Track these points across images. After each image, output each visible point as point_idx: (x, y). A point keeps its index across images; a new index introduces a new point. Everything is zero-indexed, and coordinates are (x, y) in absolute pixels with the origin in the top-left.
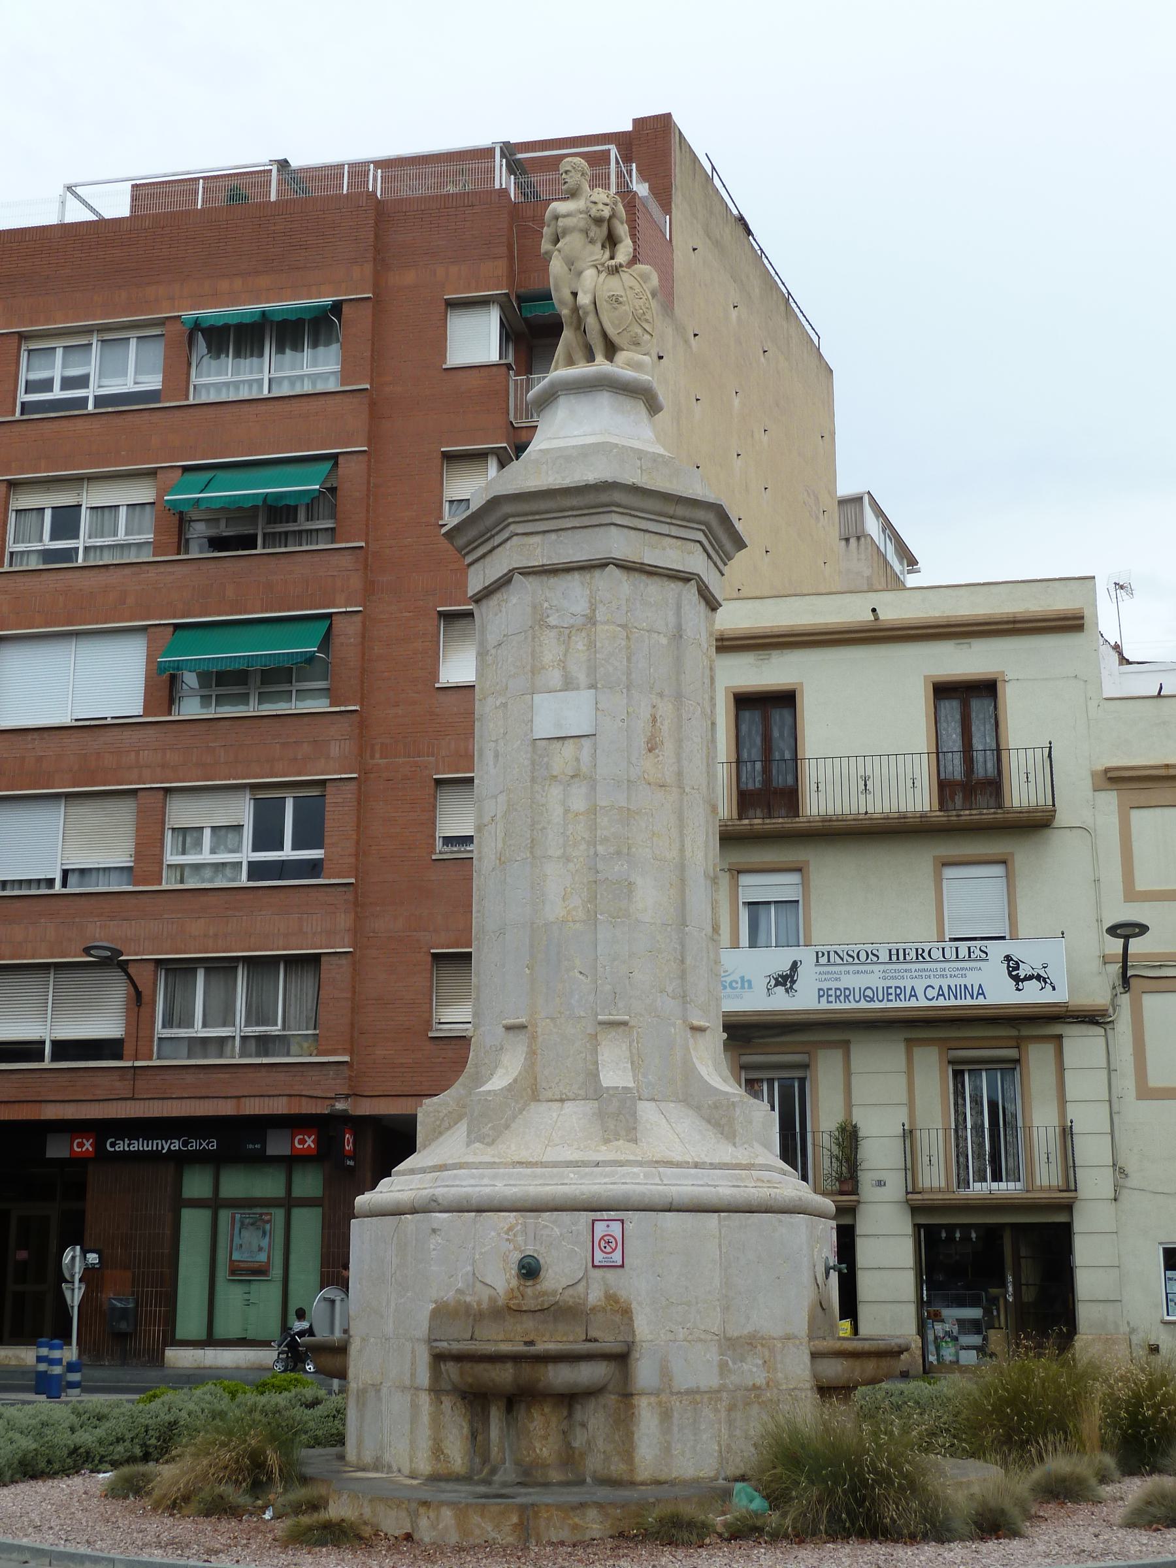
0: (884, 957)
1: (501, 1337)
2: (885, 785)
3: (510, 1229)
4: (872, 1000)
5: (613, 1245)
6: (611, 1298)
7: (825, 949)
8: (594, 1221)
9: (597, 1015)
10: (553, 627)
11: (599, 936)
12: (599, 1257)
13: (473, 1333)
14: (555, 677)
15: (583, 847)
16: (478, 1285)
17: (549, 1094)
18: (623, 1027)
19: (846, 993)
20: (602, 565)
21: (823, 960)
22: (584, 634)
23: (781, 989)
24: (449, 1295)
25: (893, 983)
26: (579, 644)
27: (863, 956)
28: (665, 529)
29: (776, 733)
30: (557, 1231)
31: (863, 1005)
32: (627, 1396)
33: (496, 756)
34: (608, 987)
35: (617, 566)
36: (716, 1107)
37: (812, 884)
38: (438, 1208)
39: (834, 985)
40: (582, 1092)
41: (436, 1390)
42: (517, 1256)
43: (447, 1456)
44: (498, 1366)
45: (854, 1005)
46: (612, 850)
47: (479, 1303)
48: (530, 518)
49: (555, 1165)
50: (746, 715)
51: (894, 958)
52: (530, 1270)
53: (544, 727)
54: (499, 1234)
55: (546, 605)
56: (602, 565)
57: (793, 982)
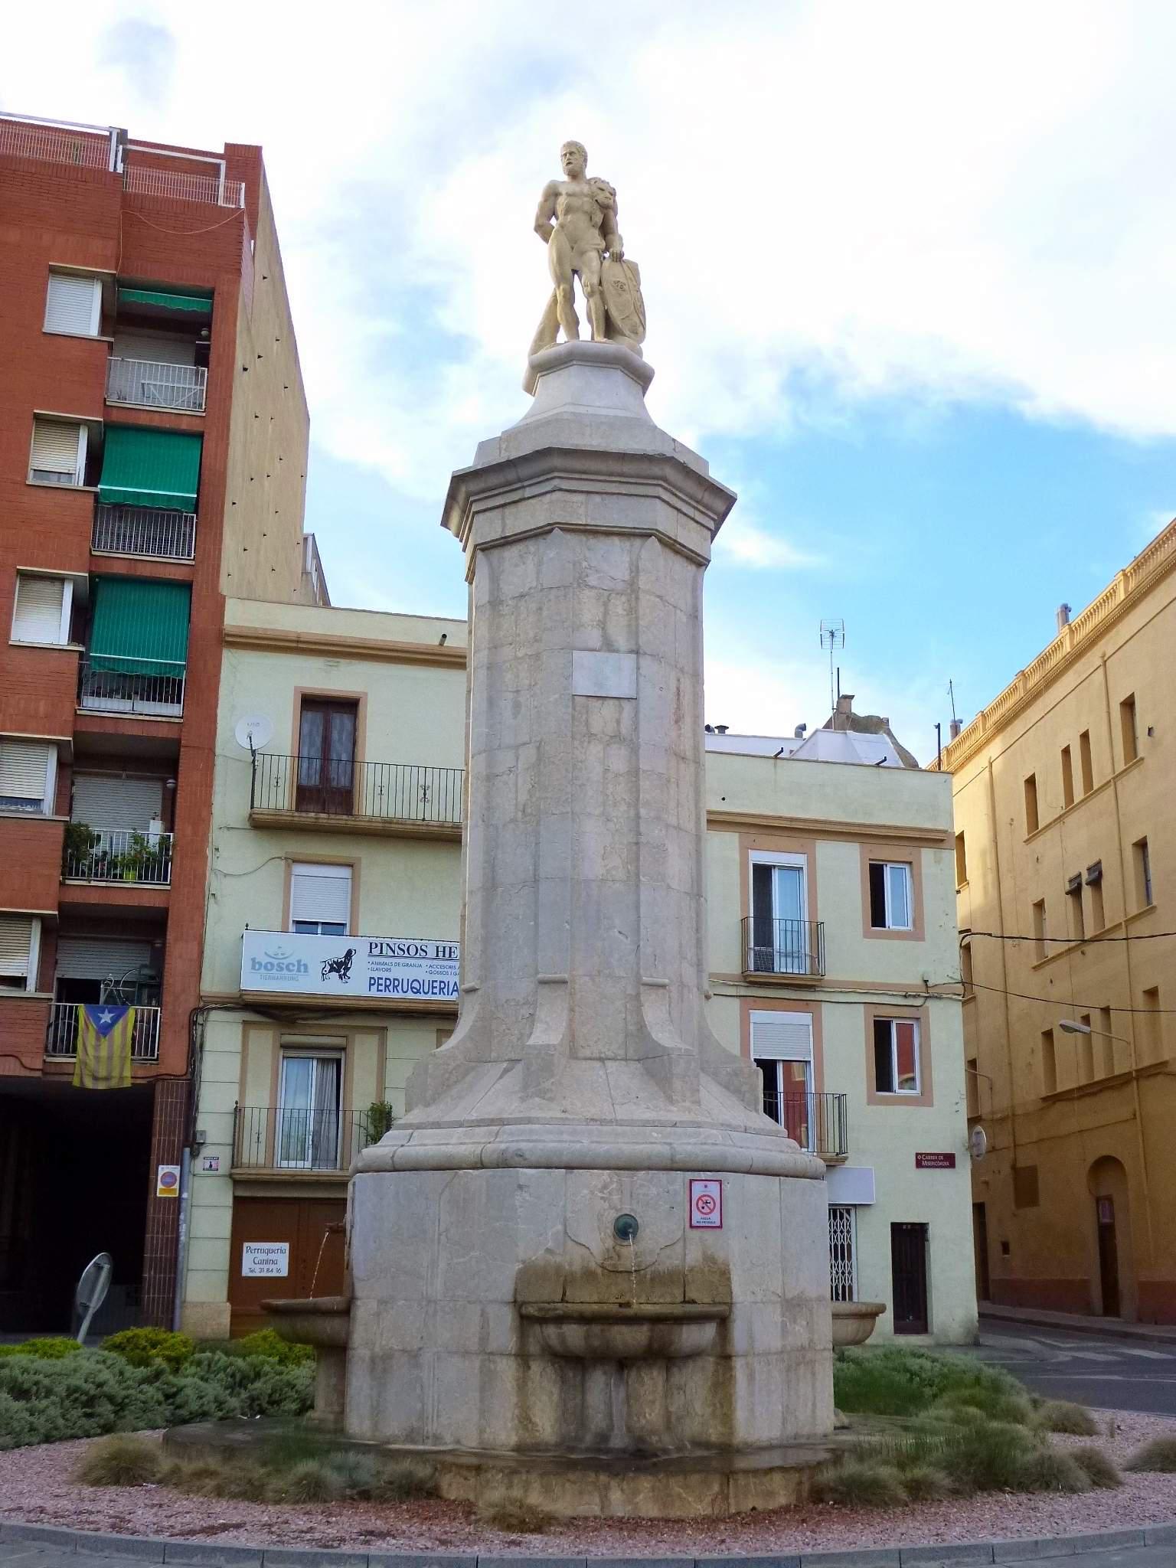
0: (432, 953)
1: (595, 1298)
2: (442, 795)
3: (605, 1187)
4: (418, 992)
5: (711, 1206)
6: (709, 1259)
7: (378, 941)
8: (691, 1181)
9: (537, 973)
10: (592, 587)
11: (642, 897)
12: (697, 1217)
13: (564, 1294)
14: (594, 637)
15: (623, 808)
16: (570, 1243)
17: (587, 1053)
18: (661, 991)
19: (394, 984)
20: (645, 535)
21: (376, 951)
22: (624, 599)
23: (335, 975)
24: (538, 1255)
25: (438, 978)
26: (619, 606)
27: (412, 951)
28: (690, 512)
29: (335, 735)
30: (654, 1191)
31: (410, 995)
32: (725, 1358)
33: (517, 706)
34: (649, 950)
35: (660, 540)
36: (736, 1075)
37: (363, 879)
38: (523, 1163)
39: (385, 975)
40: (621, 1052)
41: (523, 1357)
42: (613, 1215)
43: (534, 1424)
44: (635, 1328)
45: (401, 995)
46: (652, 814)
47: (571, 1264)
48: (577, 476)
49: (631, 1123)
50: (309, 715)
51: (441, 954)
52: (625, 1229)
53: (583, 685)
54: (592, 1193)
55: (585, 564)
56: (645, 535)
57: (347, 969)
